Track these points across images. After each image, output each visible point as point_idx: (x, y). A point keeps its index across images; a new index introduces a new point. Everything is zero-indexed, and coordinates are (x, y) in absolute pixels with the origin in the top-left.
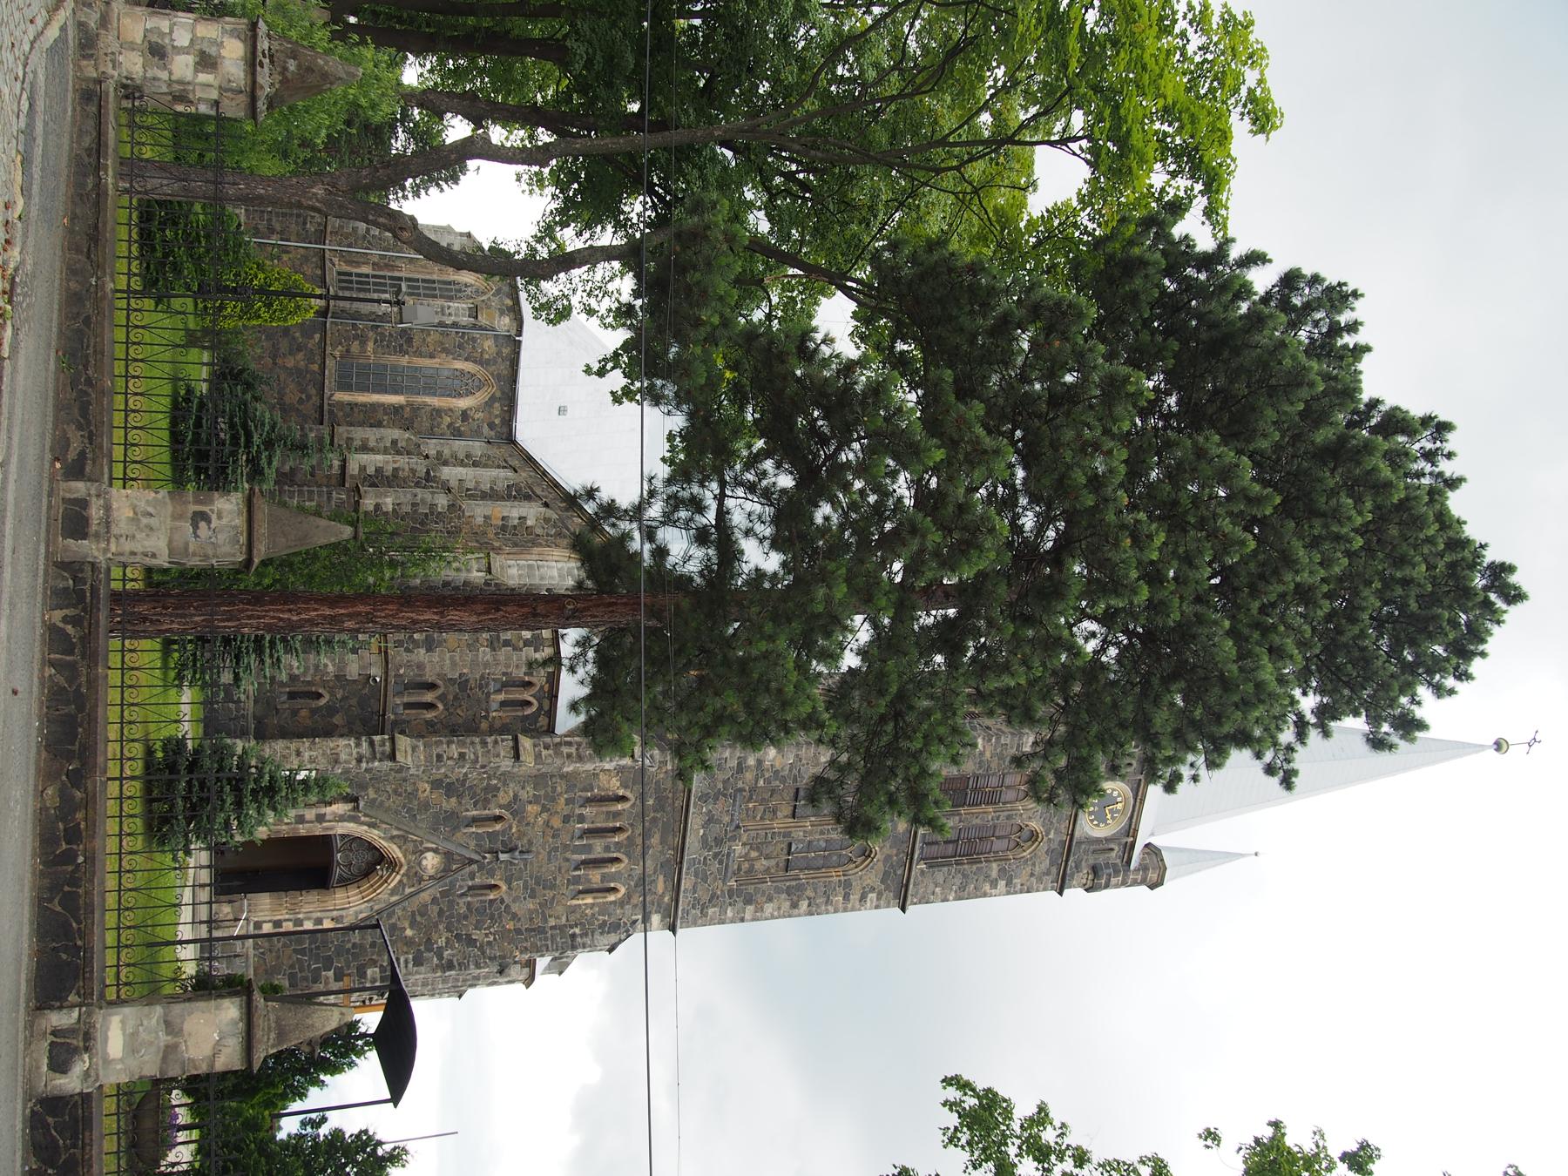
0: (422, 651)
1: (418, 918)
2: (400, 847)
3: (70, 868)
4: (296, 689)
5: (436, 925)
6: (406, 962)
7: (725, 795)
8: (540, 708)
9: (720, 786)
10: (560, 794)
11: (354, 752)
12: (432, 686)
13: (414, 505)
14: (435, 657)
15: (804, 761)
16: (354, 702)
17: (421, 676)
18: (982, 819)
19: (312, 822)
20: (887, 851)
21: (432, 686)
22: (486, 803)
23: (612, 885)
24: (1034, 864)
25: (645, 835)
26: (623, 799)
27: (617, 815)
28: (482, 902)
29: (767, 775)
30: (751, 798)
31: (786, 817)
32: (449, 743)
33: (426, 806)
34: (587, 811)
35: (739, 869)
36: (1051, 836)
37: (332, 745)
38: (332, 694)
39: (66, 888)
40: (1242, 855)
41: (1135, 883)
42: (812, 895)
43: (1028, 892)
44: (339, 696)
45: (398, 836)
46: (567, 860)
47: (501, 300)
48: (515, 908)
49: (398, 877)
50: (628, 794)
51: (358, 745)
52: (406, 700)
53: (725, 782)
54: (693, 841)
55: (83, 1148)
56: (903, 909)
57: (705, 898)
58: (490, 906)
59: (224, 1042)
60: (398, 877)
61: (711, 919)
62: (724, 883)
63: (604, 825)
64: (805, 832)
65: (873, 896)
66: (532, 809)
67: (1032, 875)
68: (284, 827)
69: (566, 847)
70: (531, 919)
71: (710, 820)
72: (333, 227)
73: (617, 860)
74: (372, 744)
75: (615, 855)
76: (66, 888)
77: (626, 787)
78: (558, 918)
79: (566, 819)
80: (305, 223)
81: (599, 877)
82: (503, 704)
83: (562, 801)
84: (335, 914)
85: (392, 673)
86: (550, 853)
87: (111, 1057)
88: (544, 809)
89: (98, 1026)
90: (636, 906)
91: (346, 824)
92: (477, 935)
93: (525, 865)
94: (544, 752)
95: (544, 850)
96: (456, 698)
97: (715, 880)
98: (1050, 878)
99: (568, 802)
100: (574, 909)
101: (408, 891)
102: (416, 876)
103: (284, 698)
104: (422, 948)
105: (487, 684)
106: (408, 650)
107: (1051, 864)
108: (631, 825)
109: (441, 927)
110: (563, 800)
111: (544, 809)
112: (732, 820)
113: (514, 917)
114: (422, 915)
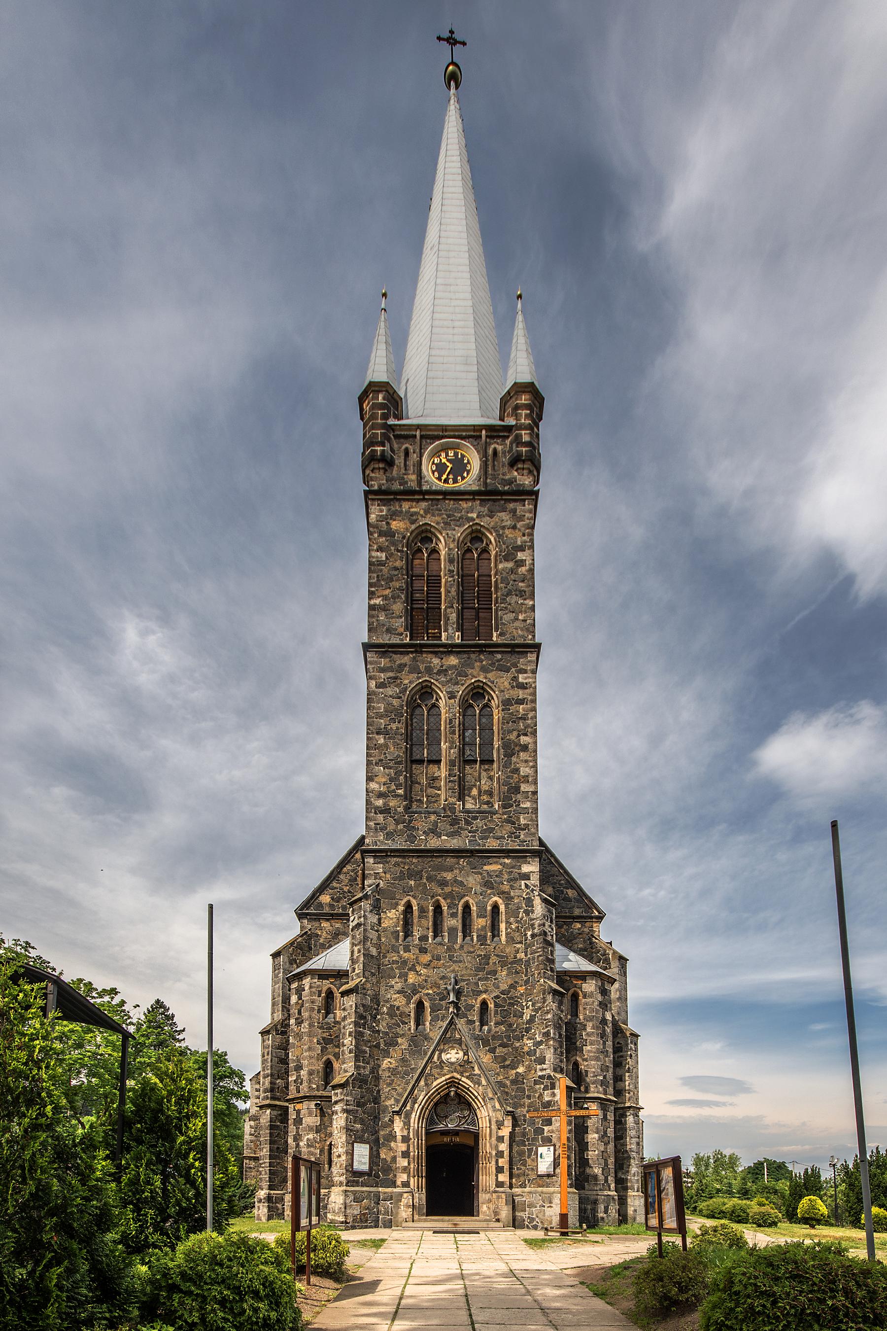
1: (508, 1063)
2: (436, 1079)
5: (516, 1049)
6: (542, 1070)
7: (410, 821)
9: (400, 827)
10: (401, 957)
11: (340, 1115)
15: (382, 757)
17: (318, 1072)
23: (489, 908)
24: (503, 528)
25: (443, 883)
26: (409, 906)
27: (423, 910)
28: (496, 1013)
29: (394, 787)
31: (439, 768)
33: (403, 1060)
34: (417, 934)
35: (488, 803)
36: (474, 515)
37: (336, 1132)
42: (515, 733)
45: (426, 1080)
46: (462, 947)
48: (504, 987)
49: (463, 1079)
53: (397, 822)
54: (454, 843)
57: (508, 827)
58: (501, 1006)
60: (463, 1079)
61: (532, 820)
62: (496, 813)
63: (431, 919)
64: (451, 748)
66: (412, 978)
67: (514, 527)
68: (412, 1166)
71: (434, 831)
72: (251, 1153)
73: (467, 907)
75: (460, 908)
77: (397, 904)
78: (517, 951)
79: (423, 950)
80: (250, 1168)
81: (480, 920)
84: (494, 1127)
86: (454, 962)
90: (512, 887)
91: (412, 1121)
92: (526, 1017)
94: (357, 971)
95: (451, 966)
97: (492, 821)
99: (407, 949)
100: (511, 939)
101: (477, 1071)
102: (465, 1066)
104: (533, 1058)
105: (328, 1023)
107: (504, 510)
108: (433, 897)
109: (518, 1045)
110: (405, 954)
111: (413, 968)
112: (434, 813)
113: (513, 986)
114: (505, 1060)
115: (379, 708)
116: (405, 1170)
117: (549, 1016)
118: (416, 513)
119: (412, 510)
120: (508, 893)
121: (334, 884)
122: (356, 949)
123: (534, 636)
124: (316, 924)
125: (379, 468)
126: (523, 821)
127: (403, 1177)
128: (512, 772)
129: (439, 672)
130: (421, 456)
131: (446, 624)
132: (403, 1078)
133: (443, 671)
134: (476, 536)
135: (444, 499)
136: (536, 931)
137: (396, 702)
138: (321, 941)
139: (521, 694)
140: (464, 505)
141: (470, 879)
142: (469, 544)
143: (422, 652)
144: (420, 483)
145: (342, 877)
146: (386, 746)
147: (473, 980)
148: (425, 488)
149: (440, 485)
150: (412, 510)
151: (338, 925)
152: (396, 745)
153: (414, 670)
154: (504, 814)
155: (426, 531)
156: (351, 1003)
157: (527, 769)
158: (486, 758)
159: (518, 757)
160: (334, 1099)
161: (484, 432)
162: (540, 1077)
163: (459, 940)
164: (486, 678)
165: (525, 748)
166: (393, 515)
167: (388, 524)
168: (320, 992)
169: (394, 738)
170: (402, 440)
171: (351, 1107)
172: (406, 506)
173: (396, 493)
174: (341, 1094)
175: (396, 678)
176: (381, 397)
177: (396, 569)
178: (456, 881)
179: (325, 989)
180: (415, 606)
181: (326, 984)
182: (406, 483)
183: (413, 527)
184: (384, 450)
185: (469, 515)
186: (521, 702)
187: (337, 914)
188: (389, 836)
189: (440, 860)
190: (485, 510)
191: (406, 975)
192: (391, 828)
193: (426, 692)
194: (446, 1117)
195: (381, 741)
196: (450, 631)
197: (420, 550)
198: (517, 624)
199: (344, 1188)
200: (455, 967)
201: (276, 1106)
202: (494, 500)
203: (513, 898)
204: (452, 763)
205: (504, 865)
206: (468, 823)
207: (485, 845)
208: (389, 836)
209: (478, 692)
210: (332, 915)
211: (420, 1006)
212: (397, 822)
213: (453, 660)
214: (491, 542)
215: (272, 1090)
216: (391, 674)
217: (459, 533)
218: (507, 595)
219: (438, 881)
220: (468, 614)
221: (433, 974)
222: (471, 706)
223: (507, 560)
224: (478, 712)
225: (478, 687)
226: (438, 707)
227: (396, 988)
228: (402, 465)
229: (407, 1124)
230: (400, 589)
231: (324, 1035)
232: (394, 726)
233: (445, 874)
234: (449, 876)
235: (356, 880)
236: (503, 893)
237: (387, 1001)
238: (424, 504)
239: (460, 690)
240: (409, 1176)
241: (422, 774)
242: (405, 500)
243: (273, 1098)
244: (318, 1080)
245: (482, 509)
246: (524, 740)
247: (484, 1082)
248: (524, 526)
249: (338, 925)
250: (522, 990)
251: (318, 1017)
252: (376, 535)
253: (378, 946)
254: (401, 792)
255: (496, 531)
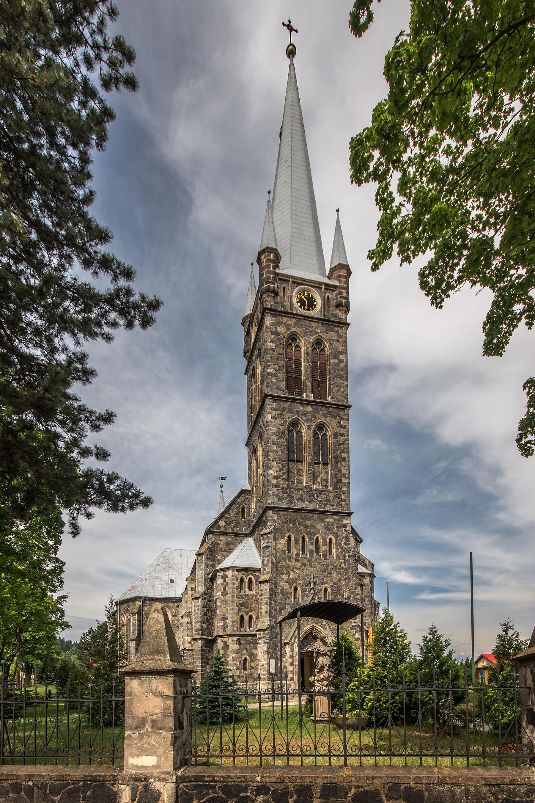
0: (228, 621)
2: (305, 626)
3: (36, 789)
4: (242, 667)
7: (290, 493)
8: (252, 575)
9: (285, 495)
12: (242, 617)
13: (188, 629)
14: (230, 616)
16: (248, 646)
18: (308, 368)
19: (293, 660)
20: (320, 416)
21: (242, 617)
22: (289, 594)
23: (328, 541)
24: (333, 340)
25: (306, 527)
26: (289, 537)
27: (297, 540)
29: (281, 474)
30: (292, 481)
32: (261, 609)
35: (325, 486)
36: (319, 331)
38: (245, 654)
39: (48, 792)
40: (338, 219)
41: (347, 283)
42: (339, 451)
43: (346, 343)
44: (246, 652)
46: (316, 560)
47: (130, 605)
48: (335, 581)
49: (318, 627)
50: (287, 535)
51: (260, 644)
52: (247, 627)
53: (284, 493)
54: (311, 506)
55: (217, 782)
56: (350, 407)
57: (337, 500)
59: (154, 690)
60: (318, 627)
61: (347, 497)
63: (301, 545)
64: (309, 456)
65: (342, 422)
66: (292, 575)
67: (338, 341)
69: (310, 561)
70: (341, 574)
71: (301, 499)
73: (317, 539)
74: (260, 638)
75: (315, 540)
76: (48, 792)
77: (284, 536)
78: (341, 563)
79: (297, 561)
81: (324, 547)
82: (250, 589)
83: (289, 563)
85: (236, 633)
86: (312, 567)
87: (156, 763)
88: (292, 570)
89: (133, 772)
90: (338, 531)
93: (317, 577)
94: (267, 571)
95: (310, 570)
96: (247, 608)
97: (329, 496)
98: (340, 331)
99: (289, 560)
100: (338, 557)
103: (246, 672)
106: (227, 627)
107: (333, 331)
108: (301, 533)
111: (292, 570)
112: (302, 489)
113: (339, 581)
115: (273, 430)
116: (292, 672)
117: (359, 597)
118: (290, 325)
119: (288, 322)
120: (337, 534)
121: (227, 515)
122: (266, 559)
123: (348, 401)
124: (217, 537)
125: (271, 296)
126: (343, 497)
127: (290, 676)
128: (338, 471)
129: (303, 414)
130: (292, 293)
131: (306, 389)
132: (289, 626)
133: (305, 414)
134: (319, 342)
135: (304, 319)
136: (351, 554)
137: (281, 428)
138: (220, 547)
139: (342, 431)
140: (314, 324)
141: (319, 525)
142: (315, 345)
143: (294, 402)
144: (292, 309)
145: (231, 511)
146: (277, 451)
147: (321, 577)
148: (294, 311)
149: (301, 311)
150: (288, 322)
151: (229, 539)
152: (282, 451)
153: (290, 411)
154: (335, 493)
155: (294, 335)
156: (266, 587)
157: (345, 471)
158: (325, 462)
159: (341, 464)
160: (258, 636)
161: (323, 286)
162: (353, 626)
163: (314, 557)
164: (325, 420)
165: (344, 459)
166: (279, 323)
167: (276, 328)
168: (237, 579)
169: (281, 447)
170: (282, 282)
171: (268, 641)
172: (285, 319)
173: (280, 312)
174: (263, 634)
175: (281, 415)
176: (272, 255)
177: (280, 354)
178: (312, 526)
179: (240, 577)
180: (289, 375)
181: (240, 575)
182: (285, 306)
183: (289, 332)
184: (274, 287)
185: (316, 330)
186: (342, 435)
187: (229, 533)
188: (280, 499)
189: (305, 514)
190: (324, 329)
191: (289, 573)
192: (280, 496)
193: (295, 424)
194: (307, 645)
195: (275, 448)
196: (308, 392)
197: (290, 344)
198: (339, 393)
199: (267, 681)
200: (312, 570)
201: (203, 638)
202: (328, 325)
203: (339, 536)
204: (310, 464)
205: (335, 519)
206: (318, 496)
207: (325, 509)
208: (280, 499)
209: (320, 427)
210: (226, 533)
211: (296, 589)
212: (284, 493)
213: (309, 409)
214: (326, 346)
215: (201, 630)
216: (279, 412)
217: (312, 339)
218: (335, 377)
219: (304, 525)
220: (316, 384)
221: (302, 573)
222: (317, 433)
223: (335, 358)
224: (320, 437)
225: (321, 424)
226: (301, 432)
227: (284, 580)
228: (282, 296)
229: (292, 649)
230: (282, 365)
231: (240, 602)
232: (281, 441)
233: (307, 522)
234: (309, 523)
235: (238, 514)
236: (335, 533)
237: (280, 586)
238: (294, 320)
239: (313, 426)
240: (293, 675)
241: (295, 467)
242: (284, 316)
243: (202, 634)
244: (237, 626)
245: (323, 328)
246: (343, 455)
247: (328, 628)
248: (343, 341)
249: (229, 539)
250: (343, 582)
251: (236, 592)
252: (270, 333)
253: (276, 558)
254: (285, 477)
255: (330, 342)
